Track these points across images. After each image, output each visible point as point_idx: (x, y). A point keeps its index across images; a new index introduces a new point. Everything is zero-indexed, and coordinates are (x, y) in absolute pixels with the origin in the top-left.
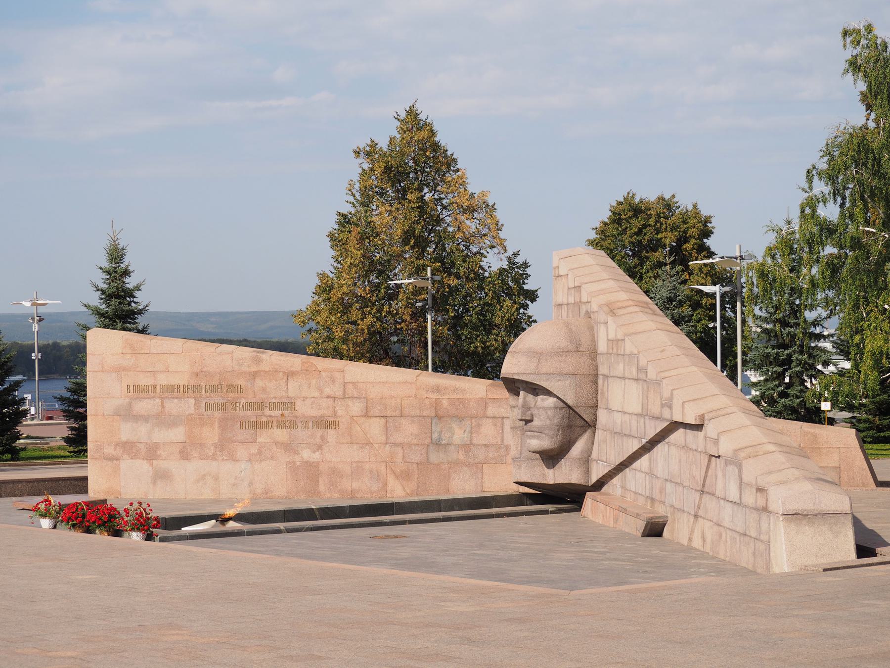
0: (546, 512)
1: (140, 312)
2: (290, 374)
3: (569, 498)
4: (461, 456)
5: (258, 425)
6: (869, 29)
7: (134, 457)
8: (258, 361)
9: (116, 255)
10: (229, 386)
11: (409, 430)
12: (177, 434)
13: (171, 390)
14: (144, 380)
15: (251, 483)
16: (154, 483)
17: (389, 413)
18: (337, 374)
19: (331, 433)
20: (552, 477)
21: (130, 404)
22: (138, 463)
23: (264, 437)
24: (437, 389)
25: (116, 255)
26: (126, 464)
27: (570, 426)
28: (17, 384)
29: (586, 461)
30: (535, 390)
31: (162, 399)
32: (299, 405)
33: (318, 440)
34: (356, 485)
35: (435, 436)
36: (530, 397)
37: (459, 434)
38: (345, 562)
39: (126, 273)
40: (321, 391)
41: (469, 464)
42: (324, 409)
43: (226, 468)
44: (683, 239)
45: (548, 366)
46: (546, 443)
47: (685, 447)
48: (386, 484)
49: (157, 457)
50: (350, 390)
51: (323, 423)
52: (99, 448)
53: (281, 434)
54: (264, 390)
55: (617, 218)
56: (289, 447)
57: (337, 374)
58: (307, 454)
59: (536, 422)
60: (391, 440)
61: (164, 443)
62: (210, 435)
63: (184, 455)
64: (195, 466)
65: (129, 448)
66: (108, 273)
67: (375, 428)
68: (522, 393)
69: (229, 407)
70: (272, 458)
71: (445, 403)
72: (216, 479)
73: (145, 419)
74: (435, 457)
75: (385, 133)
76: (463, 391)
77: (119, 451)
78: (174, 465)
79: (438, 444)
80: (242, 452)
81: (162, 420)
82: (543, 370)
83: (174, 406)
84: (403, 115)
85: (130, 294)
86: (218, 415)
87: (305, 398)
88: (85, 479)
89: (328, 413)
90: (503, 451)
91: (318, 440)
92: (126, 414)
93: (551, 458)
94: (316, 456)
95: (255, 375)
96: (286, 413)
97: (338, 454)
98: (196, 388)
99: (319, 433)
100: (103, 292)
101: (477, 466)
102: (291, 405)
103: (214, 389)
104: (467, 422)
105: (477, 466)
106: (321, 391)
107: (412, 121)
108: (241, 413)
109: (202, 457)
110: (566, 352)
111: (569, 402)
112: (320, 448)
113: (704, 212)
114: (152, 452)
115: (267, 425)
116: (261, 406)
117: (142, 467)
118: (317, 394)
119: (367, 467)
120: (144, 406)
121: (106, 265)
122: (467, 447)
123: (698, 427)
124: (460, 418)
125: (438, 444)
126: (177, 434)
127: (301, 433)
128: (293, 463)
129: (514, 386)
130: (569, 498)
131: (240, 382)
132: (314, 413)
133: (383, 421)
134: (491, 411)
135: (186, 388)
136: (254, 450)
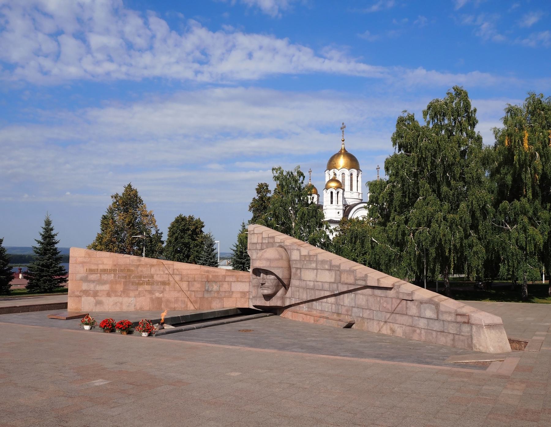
0: (266, 316)
1: (56, 243)
2: (152, 266)
3: (275, 311)
4: (216, 295)
5: (139, 284)
6: (280, 168)
7: (88, 296)
8: (140, 261)
9: (48, 223)
10: (128, 270)
11: (197, 286)
12: (106, 287)
13: (104, 271)
14: (93, 267)
15: (135, 306)
16: (96, 305)
17: (190, 280)
18: (171, 266)
19: (167, 287)
20: (268, 304)
21: (87, 276)
22: (89, 298)
23: (141, 289)
24: (208, 272)
25: (48, 223)
26: (84, 299)
27: (278, 286)
28: (11, 268)
29: (283, 298)
30: (267, 272)
31: (100, 274)
32: (155, 276)
33: (162, 289)
34: (176, 305)
35: (207, 288)
36: (265, 275)
37: (215, 287)
38: (233, 344)
39: (52, 229)
40: (164, 272)
41: (219, 298)
42: (165, 278)
43: (126, 300)
44: (197, 228)
45: (274, 264)
46: (266, 292)
47: (362, 294)
48: (187, 305)
49: (97, 296)
50: (176, 271)
51: (164, 283)
52: (73, 292)
53: (148, 287)
54: (142, 271)
55: (177, 221)
56: (150, 292)
57: (171, 266)
58: (157, 294)
59: (266, 284)
60: (190, 289)
61: (101, 291)
62: (120, 288)
63: (109, 295)
64: (113, 299)
65: (86, 293)
66: (45, 229)
67: (184, 285)
68: (262, 274)
69: (128, 277)
70: (144, 296)
71: (211, 276)
72: (121, 304)
73: (93, 281)
74: (206, 295)
75: (121, 191)
76: (217, 272)
77: (82, 294)
78: (104, 299)
79: (208, 291)
80: (132, 294)
81: (100, 282)
82: (272, 266)
83: (105, 277)
84: (127, 186)
85: (53, 237)
86: (123, 280)
87: (157, 275)
88: (66, 304)
89: (167, 280)
90: (231, 294)
91: (162, 289)
92: (85, 279)
93: (268, 297)
94: (161, 295)
95: (138, 266)
96: (150, 280)
97: (170, 294)
98: (115, 270)
99: (162, 287)
100: (43, 236)
101: (221, 299)
102: (152, 277)
103: (122, 271)
104: (218, 283)
105: (221, 299)
106: (164, 272)
107: (129, 188)
108: (132, 280)
109: (116, 296)
110: (278, 260)
111: (280, 277)
112: (162, 292)
113: (202, 221)
114: (95, 294)
115: (142, 284)
116: (140, 277)
117: (91, 300)
118: (162, 273)
119: (180, 299)
120: (93, 277)
121: (44, 226)
122: (218, 292)
123: (390, 289)
124: (216, 282)
125: (208, 291)
126: (106, 287)
127: (156, 287)
128: (152, 298)
129: (257, 272)
130: (275, 311)
131: (133, 268)
132: (160, 280)
133: (187, 283)
134: (227, 279)
135: (111, 270)
136: (137, 293)
